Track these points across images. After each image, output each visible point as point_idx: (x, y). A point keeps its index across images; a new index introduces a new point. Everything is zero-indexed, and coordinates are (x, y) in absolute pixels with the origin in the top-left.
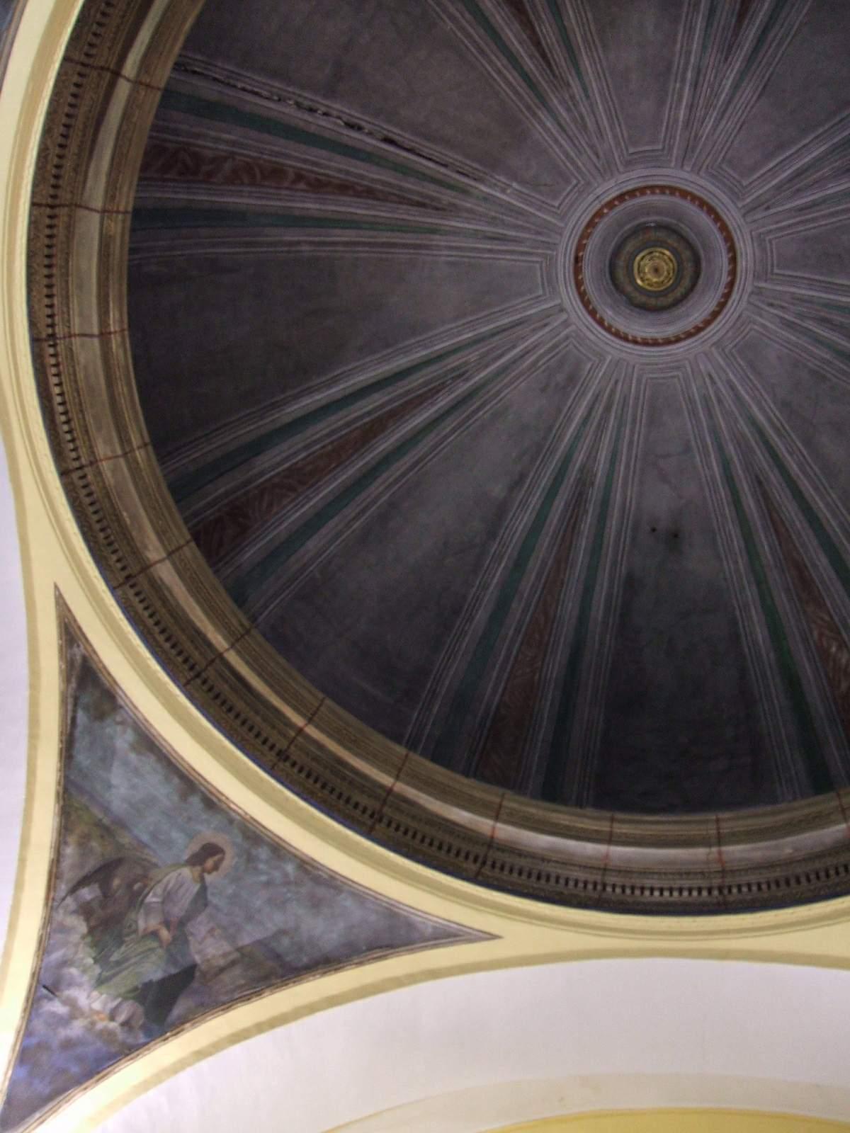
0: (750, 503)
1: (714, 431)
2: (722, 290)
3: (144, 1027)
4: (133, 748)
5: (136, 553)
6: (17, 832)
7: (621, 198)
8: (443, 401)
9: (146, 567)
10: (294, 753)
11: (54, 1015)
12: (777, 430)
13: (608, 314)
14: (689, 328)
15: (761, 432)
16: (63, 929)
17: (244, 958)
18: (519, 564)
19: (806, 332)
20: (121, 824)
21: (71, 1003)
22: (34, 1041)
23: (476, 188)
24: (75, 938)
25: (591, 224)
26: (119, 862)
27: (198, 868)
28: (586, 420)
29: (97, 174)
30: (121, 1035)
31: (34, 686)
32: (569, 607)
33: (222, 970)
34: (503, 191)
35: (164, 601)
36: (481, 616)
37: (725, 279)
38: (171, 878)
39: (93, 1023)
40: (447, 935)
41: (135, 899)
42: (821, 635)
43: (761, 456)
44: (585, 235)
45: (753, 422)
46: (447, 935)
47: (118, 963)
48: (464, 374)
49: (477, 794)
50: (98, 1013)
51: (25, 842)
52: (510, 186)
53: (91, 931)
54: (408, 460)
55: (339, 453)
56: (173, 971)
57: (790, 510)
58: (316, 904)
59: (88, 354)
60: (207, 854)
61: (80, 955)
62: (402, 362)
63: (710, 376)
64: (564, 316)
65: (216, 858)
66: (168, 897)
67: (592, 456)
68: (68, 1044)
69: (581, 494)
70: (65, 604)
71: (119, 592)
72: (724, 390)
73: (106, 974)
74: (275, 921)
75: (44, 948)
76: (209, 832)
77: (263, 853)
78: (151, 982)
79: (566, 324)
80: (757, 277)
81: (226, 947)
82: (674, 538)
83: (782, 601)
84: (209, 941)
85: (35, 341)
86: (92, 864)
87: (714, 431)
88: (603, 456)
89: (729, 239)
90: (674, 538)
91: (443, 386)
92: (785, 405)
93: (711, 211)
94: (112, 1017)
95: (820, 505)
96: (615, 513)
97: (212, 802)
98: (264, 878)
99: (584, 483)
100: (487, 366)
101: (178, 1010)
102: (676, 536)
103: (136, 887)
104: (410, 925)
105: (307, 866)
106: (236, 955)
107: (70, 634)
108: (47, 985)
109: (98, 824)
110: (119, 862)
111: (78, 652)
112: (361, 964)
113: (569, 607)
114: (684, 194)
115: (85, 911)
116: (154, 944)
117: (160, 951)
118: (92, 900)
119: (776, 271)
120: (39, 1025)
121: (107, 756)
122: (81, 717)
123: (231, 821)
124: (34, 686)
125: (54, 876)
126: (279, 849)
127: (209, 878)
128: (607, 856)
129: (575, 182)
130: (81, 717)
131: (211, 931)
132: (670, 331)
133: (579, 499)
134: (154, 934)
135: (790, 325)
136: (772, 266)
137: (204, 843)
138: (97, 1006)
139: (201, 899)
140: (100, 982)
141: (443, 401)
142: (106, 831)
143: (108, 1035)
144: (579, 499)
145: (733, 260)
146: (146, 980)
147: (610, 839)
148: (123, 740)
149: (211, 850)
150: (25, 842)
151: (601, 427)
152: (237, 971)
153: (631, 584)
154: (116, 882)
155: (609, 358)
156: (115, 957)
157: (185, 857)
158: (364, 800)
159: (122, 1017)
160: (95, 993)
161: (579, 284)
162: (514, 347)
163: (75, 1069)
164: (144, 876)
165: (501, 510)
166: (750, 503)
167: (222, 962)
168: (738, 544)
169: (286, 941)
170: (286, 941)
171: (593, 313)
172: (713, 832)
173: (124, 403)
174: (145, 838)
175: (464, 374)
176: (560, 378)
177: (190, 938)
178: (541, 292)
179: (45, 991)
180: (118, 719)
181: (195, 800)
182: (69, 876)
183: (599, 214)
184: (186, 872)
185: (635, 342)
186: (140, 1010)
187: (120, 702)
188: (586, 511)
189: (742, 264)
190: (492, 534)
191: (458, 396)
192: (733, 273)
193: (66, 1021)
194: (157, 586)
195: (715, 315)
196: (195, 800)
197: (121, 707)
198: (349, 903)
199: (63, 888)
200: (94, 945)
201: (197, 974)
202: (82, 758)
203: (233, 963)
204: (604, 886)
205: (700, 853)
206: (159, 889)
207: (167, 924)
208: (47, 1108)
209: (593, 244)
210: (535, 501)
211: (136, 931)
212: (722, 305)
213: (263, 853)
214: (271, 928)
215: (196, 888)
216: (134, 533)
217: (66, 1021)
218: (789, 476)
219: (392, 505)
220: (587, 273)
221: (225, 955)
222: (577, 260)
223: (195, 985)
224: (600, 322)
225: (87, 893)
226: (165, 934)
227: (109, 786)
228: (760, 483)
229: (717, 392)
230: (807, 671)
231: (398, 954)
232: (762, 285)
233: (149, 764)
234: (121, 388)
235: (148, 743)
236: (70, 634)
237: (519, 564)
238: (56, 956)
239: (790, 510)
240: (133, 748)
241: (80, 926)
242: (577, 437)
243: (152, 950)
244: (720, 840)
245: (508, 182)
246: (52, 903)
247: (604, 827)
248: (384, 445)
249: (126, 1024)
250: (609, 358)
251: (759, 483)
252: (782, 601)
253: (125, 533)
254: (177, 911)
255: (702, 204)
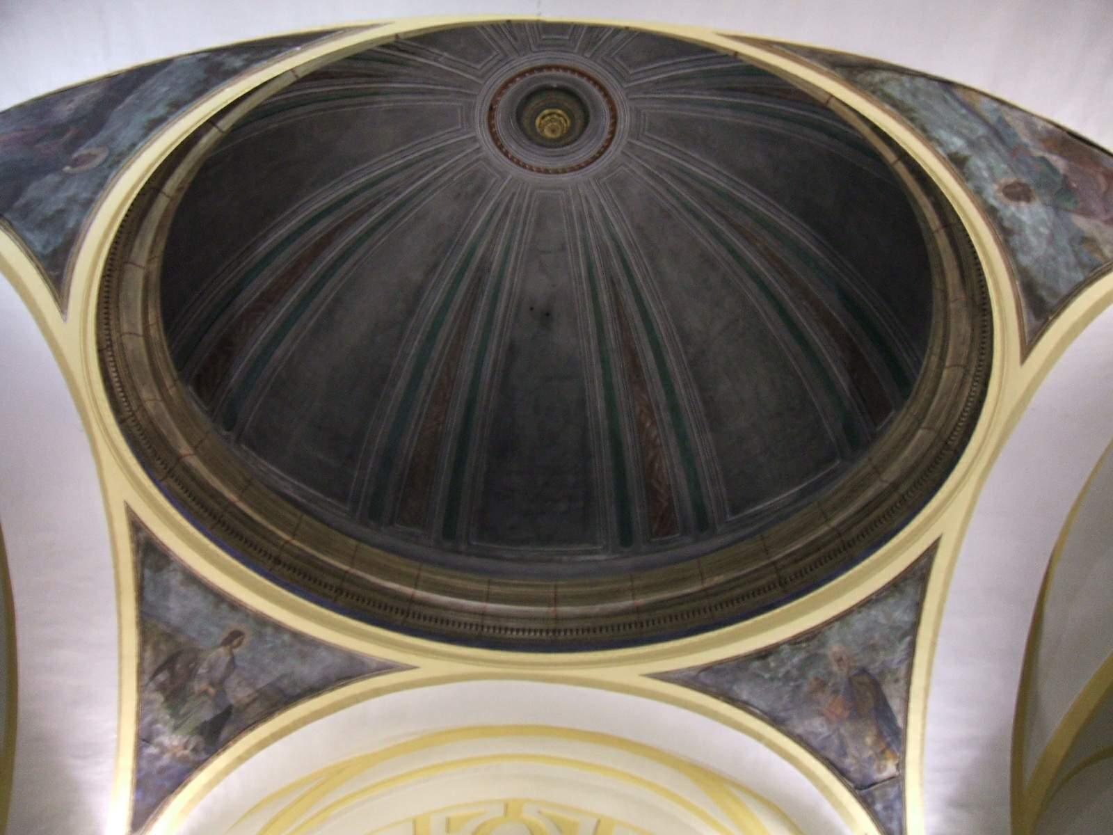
0: (604, 298)
1: (585, 240)
2: (602, 142)
3: (205, 749)
4: (182, 583)
5: (172, 451)
6: (116, 654)
7: (531, 71)
8: (378, 213)
9: (179, 458)
10: (284, 556)
11: (151, 755)
12: (630, 245)
13: (513, 148)
14: (574, 164)
15: (619, 248)
16: (149, 702)
17: (261, 695)
18: (432, 336)
19: (662, 182)
20: (178, 630)
21: (160, 745)
22: (143, 773)
23: (415, 60)
24: (157, 706)
25: (505, 86)
26: (179, 654)
27: (228, 647)
28: (488, 223)
29: (141, 245)
30: (192, 757)
31: (116, 565)
32: (465, 372)
33: (248, 705)
34: (435, 60)
35: (194, 479)
36: (401, 384)
37: (606, 135)
38: (212, 655)
39: (174, 755)
40: (386, 668)
41: (191, 674)
42: (642, 411)
43: (615, 263)
44: (500, 93)
45: (614, 238)
46: (386, 668)
47: (185, 715)
48: (394, 191)
49: (404, 569)
50: (176, 747)
51: (120, 657)
52: (441, 56)
53: (167, 699)
54: (351, 261)
55: (294, 273)
56: (219, 712)
57: (631, 308)
58: (303, 656)
59: (135, 346)
60: (234, 637)
61: (162, 715)
62: (348, 188)
63: (586, 198)
64: (477, 145)
65: (239, 639)
66: (211, 668)
67: (490, 250)
68: (162, 770)
69: (480, 279)
70: (56, 300)
71: (163, 483)
72: (596, 211)
73: (179, 722)
74: (280, 669)
75: (140, 718)
76: (234, 623)
77: (269, 631)
78: (205, 722)
79: (478, 150)
80: (631, 135)
81: (249, 691)
82: (546, 317)
83: (618, 379)
84: (238, 689)
85: (100, 351)
86: (162, 659)
87: (585, 240)
88: (499, 249)
89: (613, 109)
90: (546, 317)
91: (378, 201)
92: (639, 229)
93: (602, 88)
94: (185, 748)
95: (654, 310)
96: (504, 297)
97: (236, 606)
98: (270, 645)
99: (483, 269)
100: (413, 183)
101: (225, 733)
102: (548, 314)
103: (192, 665)
104: (363, 663)
105: (297, 636)
106: (257, 695)
107: (136, 526)
108: (144, 737)
109: (163, 634)
110: (179, 654)
111: (142, 535)
112: (333, 690)
113: (465, 372)
114: (582, 74)
115: (161, 688)
116: (204, 698)
117: (210, 702)
118: (164, 681)
119: (646, 133)
120: (144, 764)
121: (166, 592)
122: (148, 573)
123: (248, 615)
124: (116, 565)
125: (141, 672)
126: (279, 628)
127: (236, 651)
128: (485, 607)
129: (495, 53)
130: (148, 573)
131: (239, 684)
132: (560, 164)
133: (479, 281)
134: (205, 693)
135: (651, 174)
136: (644, 129)
137: (232, 630)
138: (176, 743)
139: (232, 664)
140: (176, 728)
141: (378, 213)
142: (170, 636)
143: (184, 759)
144: (479, 281)
145: (614, 124)
146: (203, 720)
147: (488, 598)
148: (175, 580)
149: (236, 635)
150: (120, 657)
151: (499, 227)
152: (257, 705)
153: (512, 351)
154: (178, 666)
155: (509, 177)
156: (182, 712)
157: (220, 641)
158: (330, 580)
159: (191, 746)
160: (174, 736)
161: (491, 127)
162: (435, 168)
163: (168, 784)
164: (195, 657)
165: (419, 291)
166: (604, 298)
167: (247, 700)
168: (592, 329)
169: (286, 681)
170: (286, 681)
171: (500, 147)
172: (552, 595)
173: (160, 364)
174: (194, 635)
175: (394, 191)
176: (470, 188)
177: (227, 690)
178: (460, 127)
179: (143, 743)
180: (171, 568)
181: (224, 607)
182: (150, 669)
183: (512, 80)
184: (221, 650)
185: (531, 169)
186: (201, 739)
187: (172, 559)
188: (483, 292)
189: (621, 126)
190: (410, 312)
191: (388, 209)
192: (613, 133)
193: (157, 757)
194: (187, 469)
195: (595, 159)
196: (224, 607)
197: (172, 561)
198: (324, 654)
199: (146, 678)
200: (169, 707)
201: (233, 711)
202: (150, 597)
203: (254, 700)
204: (483, 627)
205: (542, 610)
206: (205, 665)
207: (212, 684)
208: (155, 812)
209: (503, 101)
210: (445, 284)
211: (193, 693)
212: (601, 153)
213: (269, 631)
214: (276, 674)
215: (228, 659)
216: (170, 440)
217: (157, 757)
218: (635, 285)
219: (338, 300)
220: (499, 117)
221: (249, 696)
222: (491, 109)
223: (232, 717)
224: (506, 154)
225: (161, 677)
226: (212, 691)
227: (168, 609)
228: (613, 282)
229: (590, 209)
230: (628, 438)
231: (357, 681)
232: (634, 142)
233: (192, 590)
234: (158, 354)
235: (192, 579)
236: (136, 526)
237: (432, 336)
238: (148, 719)
239: (631, 308)
240: (182, 583)
241: (159, 698)
242: (481, 235)
243: (203, 703)
244: (556, 601)
245: (441, 53)
246: (141, 689)
247: (483, 588)
248: (330, 255)
249: (195, 750)
250: (509, 177)
251: (613, 282)
252: (618, 379)
253: (162, 439)
254: (218, 675)
255: (596, 83)
